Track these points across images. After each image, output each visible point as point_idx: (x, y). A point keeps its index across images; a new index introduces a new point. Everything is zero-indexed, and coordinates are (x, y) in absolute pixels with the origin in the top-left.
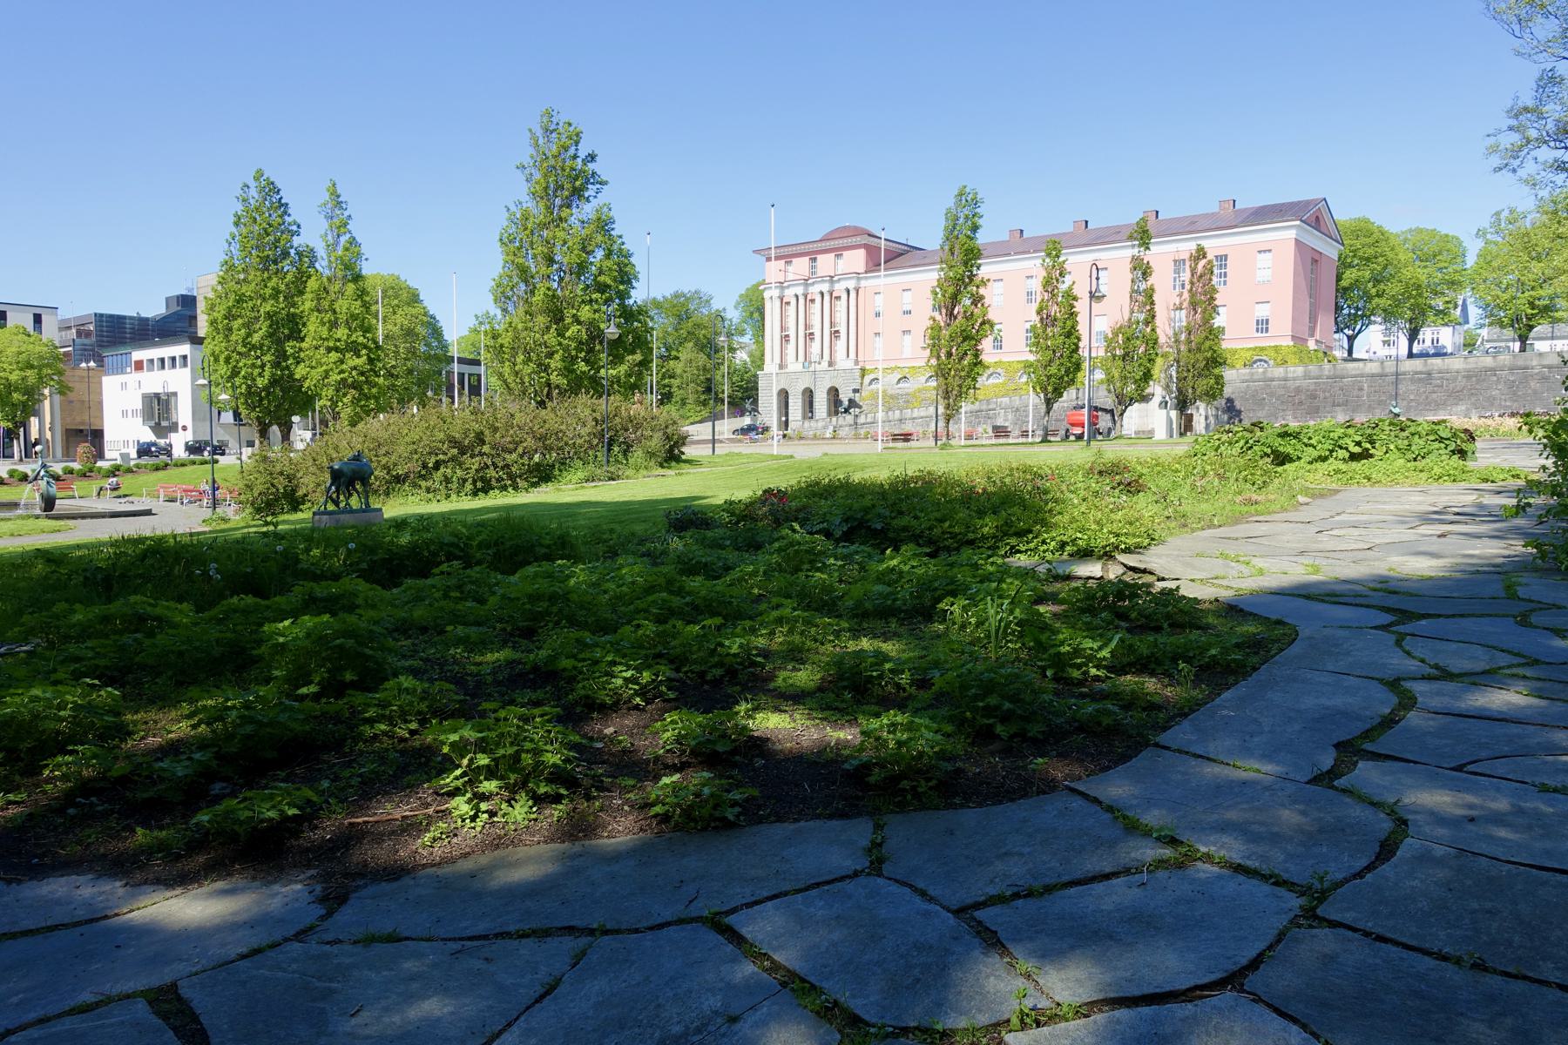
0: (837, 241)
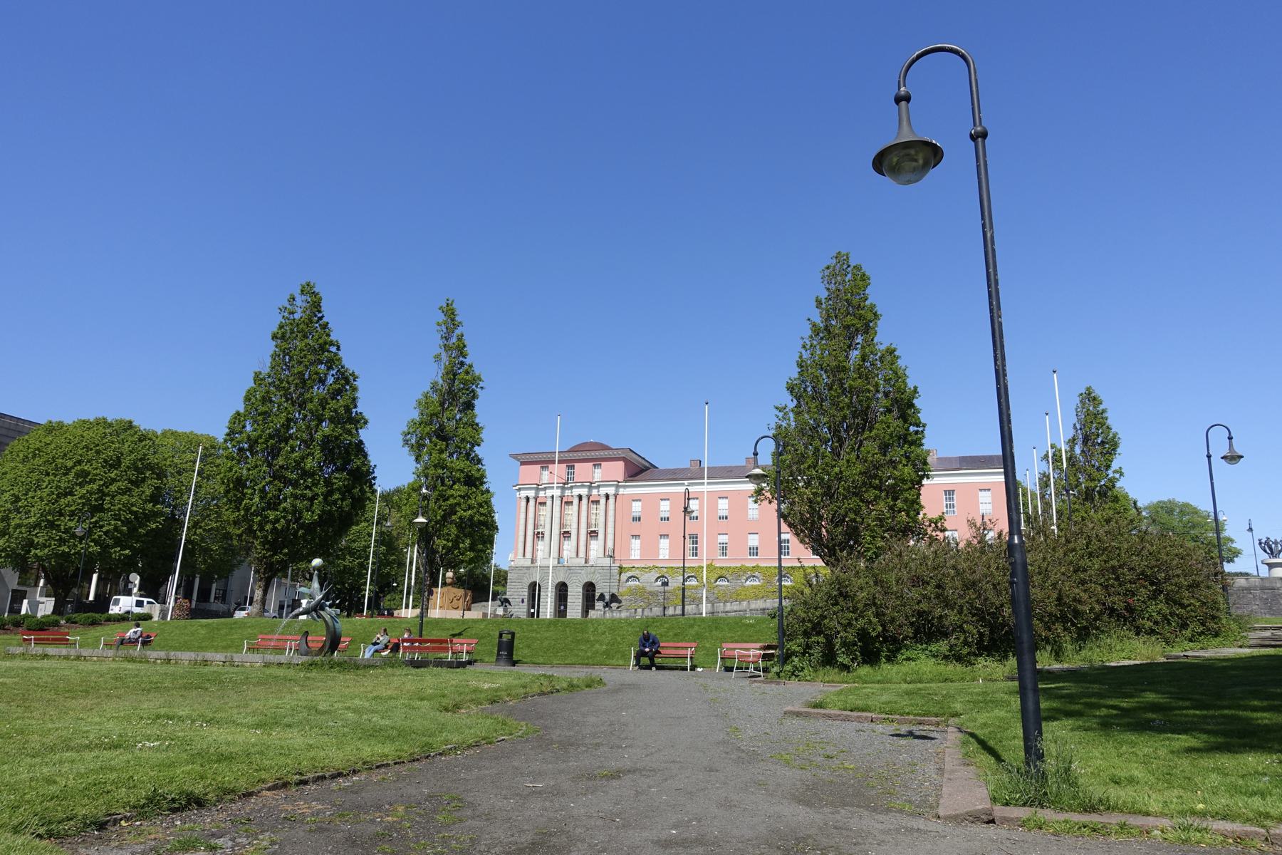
0: (594, 453)
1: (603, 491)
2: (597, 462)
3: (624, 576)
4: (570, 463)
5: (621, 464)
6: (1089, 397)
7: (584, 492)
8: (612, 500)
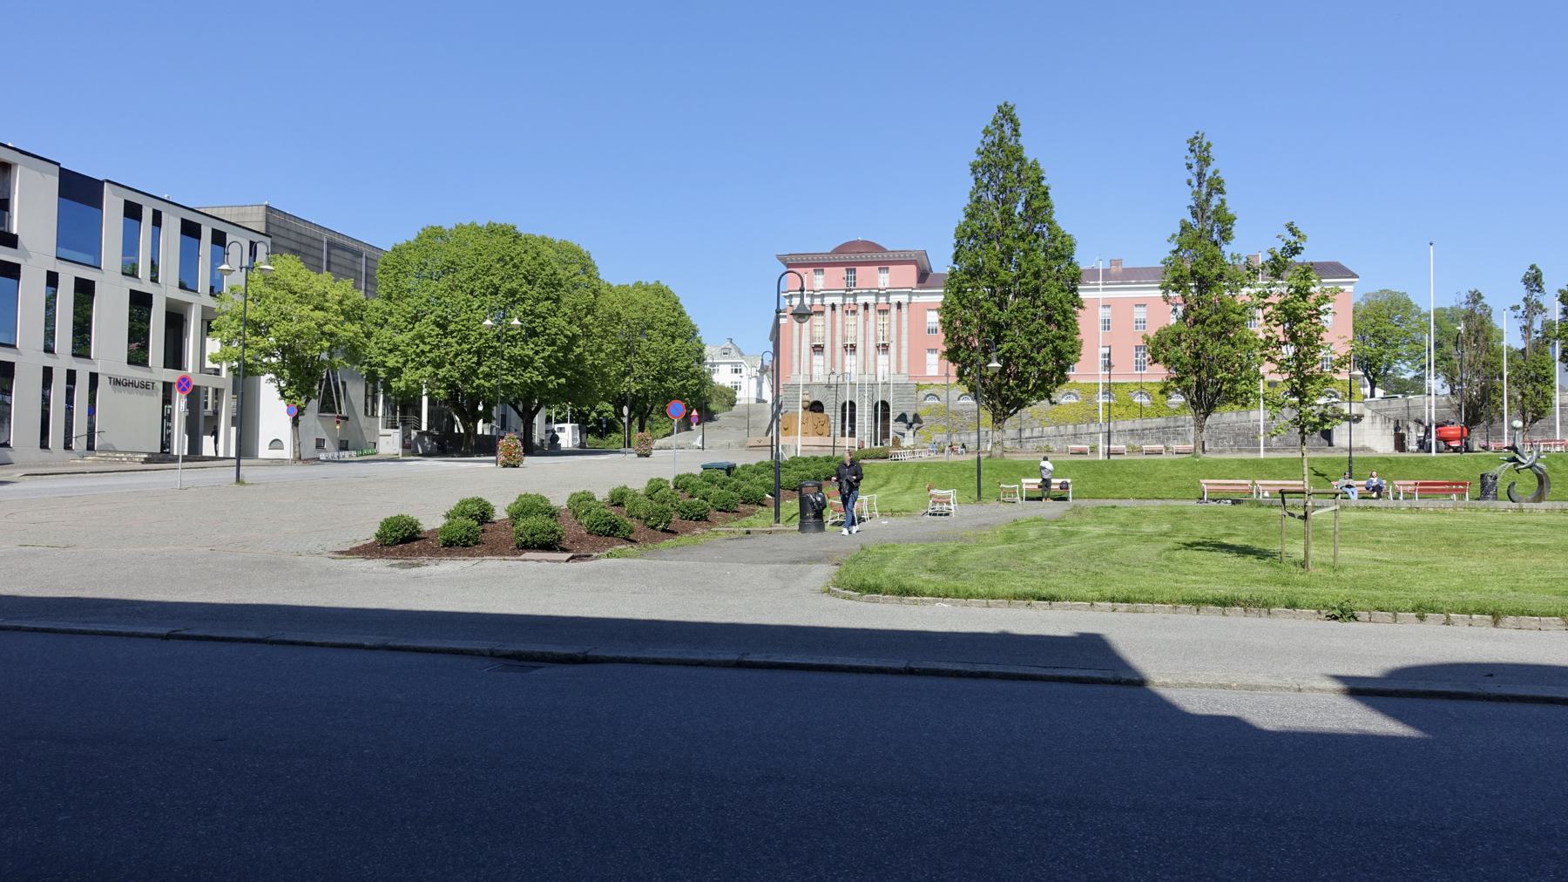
1: (894, 299)
2: (884, 265)
3: (922, 394)
4: (851, 266)
5: (913, 267)
6: (1006, 114)
7: (871, 300)
8: (904, 309)
